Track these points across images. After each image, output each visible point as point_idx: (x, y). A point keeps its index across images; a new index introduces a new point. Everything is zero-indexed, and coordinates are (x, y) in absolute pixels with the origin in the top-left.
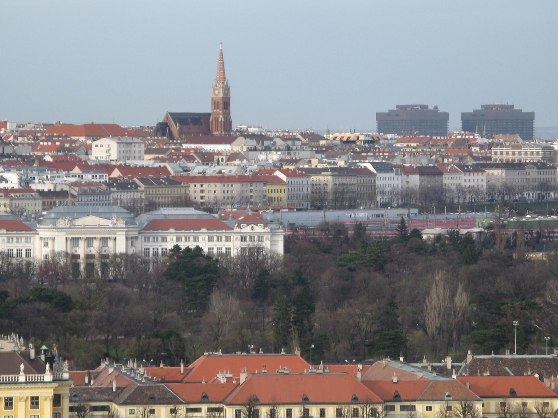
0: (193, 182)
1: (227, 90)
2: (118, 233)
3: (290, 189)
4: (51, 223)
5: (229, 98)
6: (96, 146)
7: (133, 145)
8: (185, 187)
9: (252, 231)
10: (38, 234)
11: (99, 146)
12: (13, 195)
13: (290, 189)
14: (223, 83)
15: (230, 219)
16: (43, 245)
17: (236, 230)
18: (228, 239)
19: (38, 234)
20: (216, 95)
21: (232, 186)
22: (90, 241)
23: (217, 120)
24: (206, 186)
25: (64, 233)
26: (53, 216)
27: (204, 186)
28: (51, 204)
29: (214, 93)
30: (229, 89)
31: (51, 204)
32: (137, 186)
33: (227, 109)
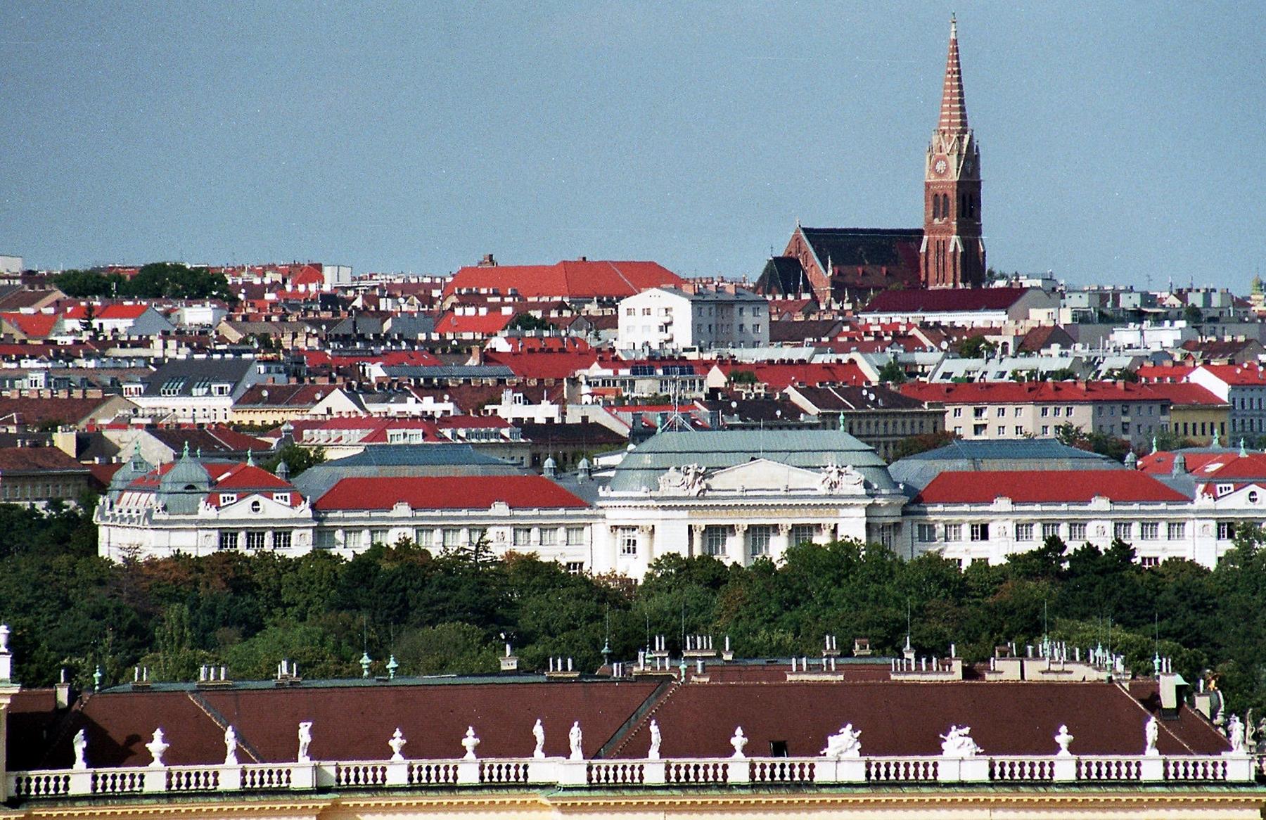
0: (954, 403)
1: (970, 161)
2: (843, 512)
3: (1238, 421)
4: (643, 482)
5: (978, 185)
6: (629, 312)
7: (736, 309)
8: (935, 414)
9: (1251, 506)
10: (604, 517)
11: (639, 312)
12: (447, 433)
13: (1238, 421)
14: (960, 139)
15: (1176, 471)
16: (620, 551)
17: (1202, 501)
18: (1176, 527)
19: (604, 517)
20: (940, 175)
21: (1069, 412)
22: (758, 534)
23: (941, 248)
24: (990, 412)
25: (685, 514)
26: (647, 460)
27: (985, 415)
28: (565, 459)
29: (934, 169)
30: (977, 157)
31: (565, 459)
32: (796, 410)
33: (971, 215)
